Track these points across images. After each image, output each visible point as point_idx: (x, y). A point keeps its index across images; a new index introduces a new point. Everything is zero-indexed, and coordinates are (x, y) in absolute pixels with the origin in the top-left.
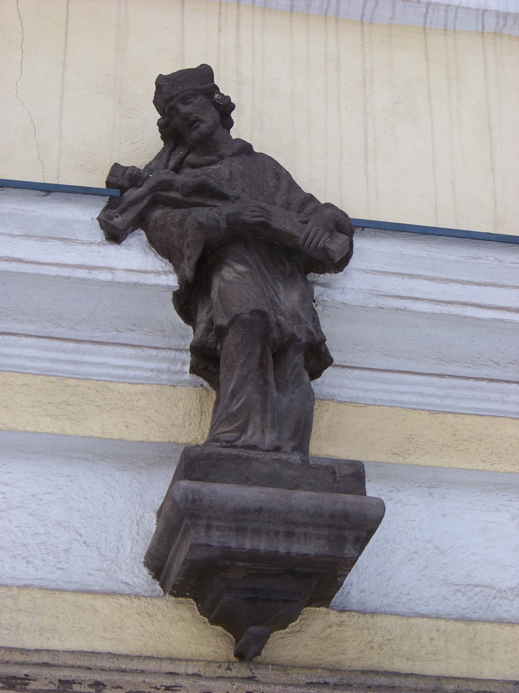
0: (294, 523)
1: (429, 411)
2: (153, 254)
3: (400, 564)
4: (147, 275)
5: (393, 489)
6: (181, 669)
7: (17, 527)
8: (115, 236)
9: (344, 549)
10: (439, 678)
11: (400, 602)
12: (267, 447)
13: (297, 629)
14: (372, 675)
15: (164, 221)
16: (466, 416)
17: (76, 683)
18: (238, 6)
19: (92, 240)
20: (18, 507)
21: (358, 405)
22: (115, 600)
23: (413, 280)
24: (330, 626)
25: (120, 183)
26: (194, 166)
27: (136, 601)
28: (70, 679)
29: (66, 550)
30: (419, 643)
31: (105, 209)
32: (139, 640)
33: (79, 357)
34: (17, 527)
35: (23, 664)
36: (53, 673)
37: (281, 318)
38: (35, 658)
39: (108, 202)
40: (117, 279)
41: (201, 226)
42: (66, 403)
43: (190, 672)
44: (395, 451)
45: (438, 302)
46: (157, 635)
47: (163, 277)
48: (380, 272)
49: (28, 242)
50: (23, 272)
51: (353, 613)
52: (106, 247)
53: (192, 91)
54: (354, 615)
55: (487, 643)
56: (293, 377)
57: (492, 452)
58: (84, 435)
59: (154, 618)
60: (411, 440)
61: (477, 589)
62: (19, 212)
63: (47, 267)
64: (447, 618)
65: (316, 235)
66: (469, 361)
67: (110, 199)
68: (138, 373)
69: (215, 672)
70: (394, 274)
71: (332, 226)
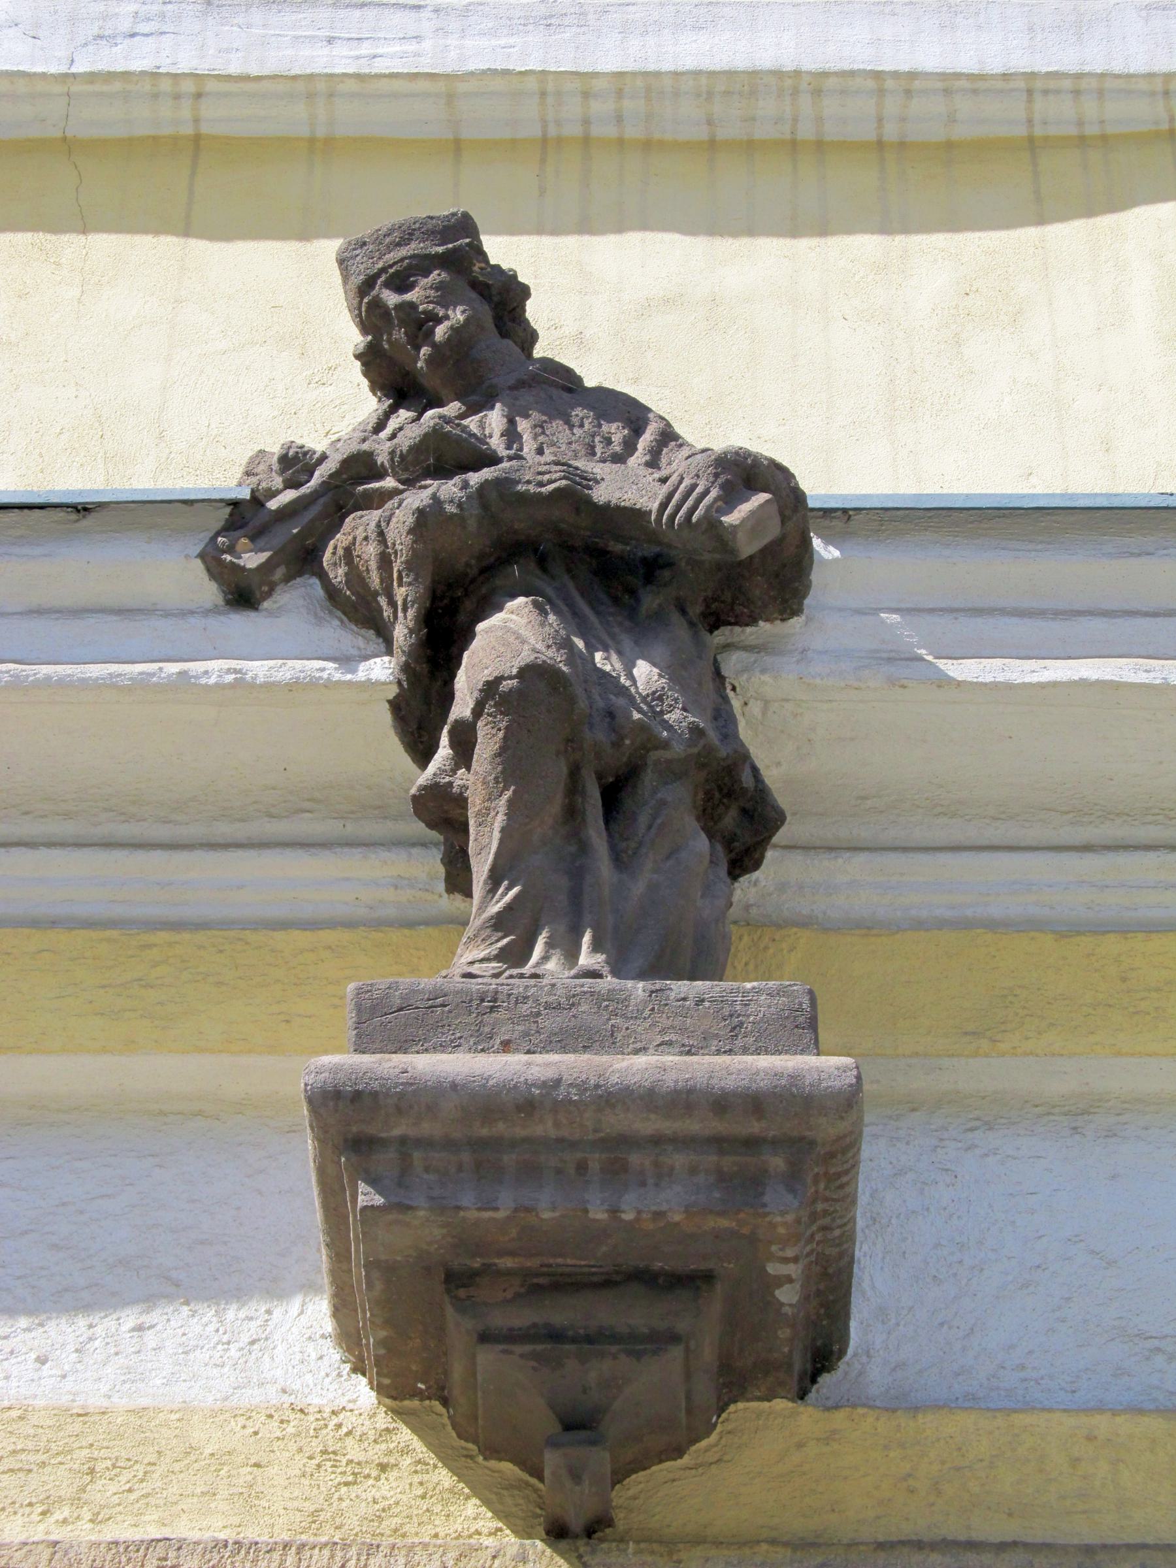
2: (336, 622)
3: (997, 1297)
5: (977, 1123)
9: (763, 1194)
11: (998, 1388)
13: (711, 1456)
15: (350, 538)
30: (1041, 1471)
52: (222, 618)
54: (864, 1415)
66: (1157, 811)
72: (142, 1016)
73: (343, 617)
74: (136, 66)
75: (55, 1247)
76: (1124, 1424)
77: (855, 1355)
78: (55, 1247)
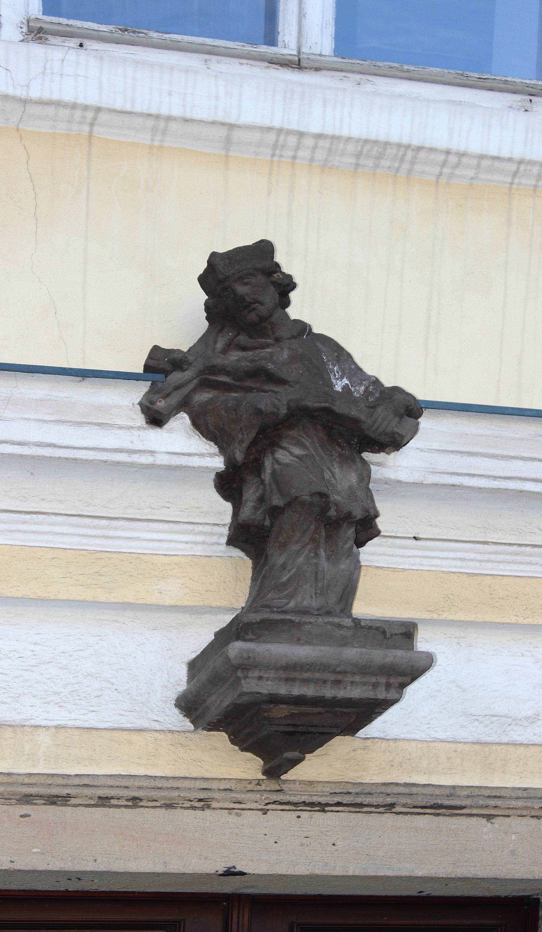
1: (467, 573)
6: (214, 785)
7: (49, 679)
8: (156, 419)
10: (454, 787)
14: (392, 786)
16: (505, 578)
17: (114, 799)
19: (132, 424)
21: (396, 570)
22: (151, 735)
23: (472, 458)
24: (355, 750)
25: (161, 366)
26: (244, 349)
27: (170, 735)
28: (109, 796)
31: (147, 393)
32: (173, 765)
33: (111, 533)
34: (49, 679)
36: (93, 792)
38: (77, 781)
39: (150, 387)
40: (159, 462)
41: (259, 412)
42: (99, 574)
43: (222, 787)
44: (429, 609)
45: (495, 478)
46: (190, 761)
47: (208, 459)
48: (438, 450)
49: (62, 427)
50: (58, 456)
51: (376, 740)
52: (146, 431)
53: (251, 271)
55: (501, 760)
57: (527, 608)
58: (117, 601)
59: (186, 748)
60: (447, 599)
61: (494, 719)
62: (52, 398)
63: (84, 452)
67: (152, 384)
69: (245, 787)
70: (452, 452)
71: (402, 411)
72: (100, 587)
73: (200, 435)
74: (68, 96)
75: (61, 668)
76: (467, 747)
78: (61, 668)
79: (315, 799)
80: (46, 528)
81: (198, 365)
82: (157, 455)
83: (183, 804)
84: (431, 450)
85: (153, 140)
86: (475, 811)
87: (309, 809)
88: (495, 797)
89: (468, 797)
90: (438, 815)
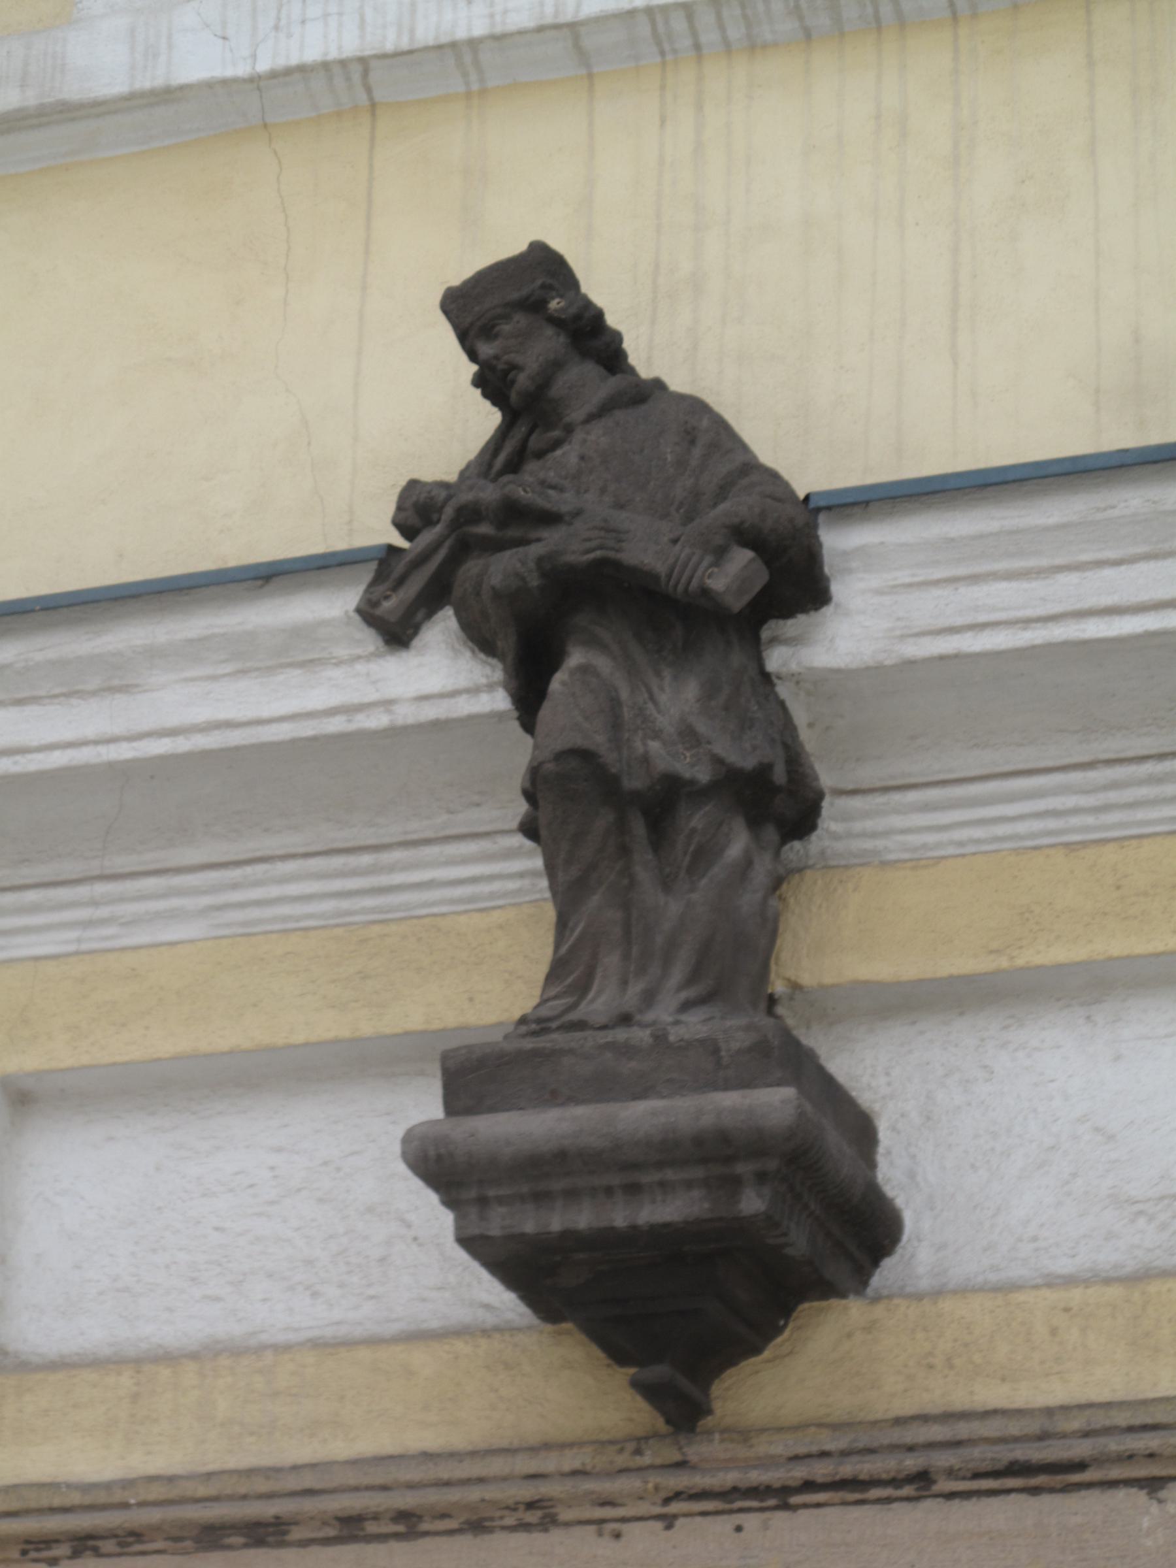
0: (635, 1166)
2: (468, 654)
4: (453, 701)
6: (549, 1463)
7: (297, 1229)
8: (397, 634)
12: (602, 1019)
16: (1145, 842)
18: (699, 107)
20: (299, 1190)
21: (923, 862)
27: (483, 1342)
29: (382, 1260)
35: (270, 1496)
37: (654, 746)
38: (292, 1483)
40: (400, 721)
43: (567, 1468)
45: (1027, 622)
56: (688, 859)
64: (1070, 1281)
65: (685, 565)
68: (496, 886)
74: (312, 55)
75: (321, 1201)
77: (909, 1240)
79: (756, 1477)
80: (274, 891)
81: (449, 512)
82: (395, 708)
83: (501, 1518)
84: (894, 589)
85: (467, 83)
86: (1115, 1473)
87: (755, 1504)
88: (1145, 1428)
89: (1086, 1434)
90: (1035, 1491)
